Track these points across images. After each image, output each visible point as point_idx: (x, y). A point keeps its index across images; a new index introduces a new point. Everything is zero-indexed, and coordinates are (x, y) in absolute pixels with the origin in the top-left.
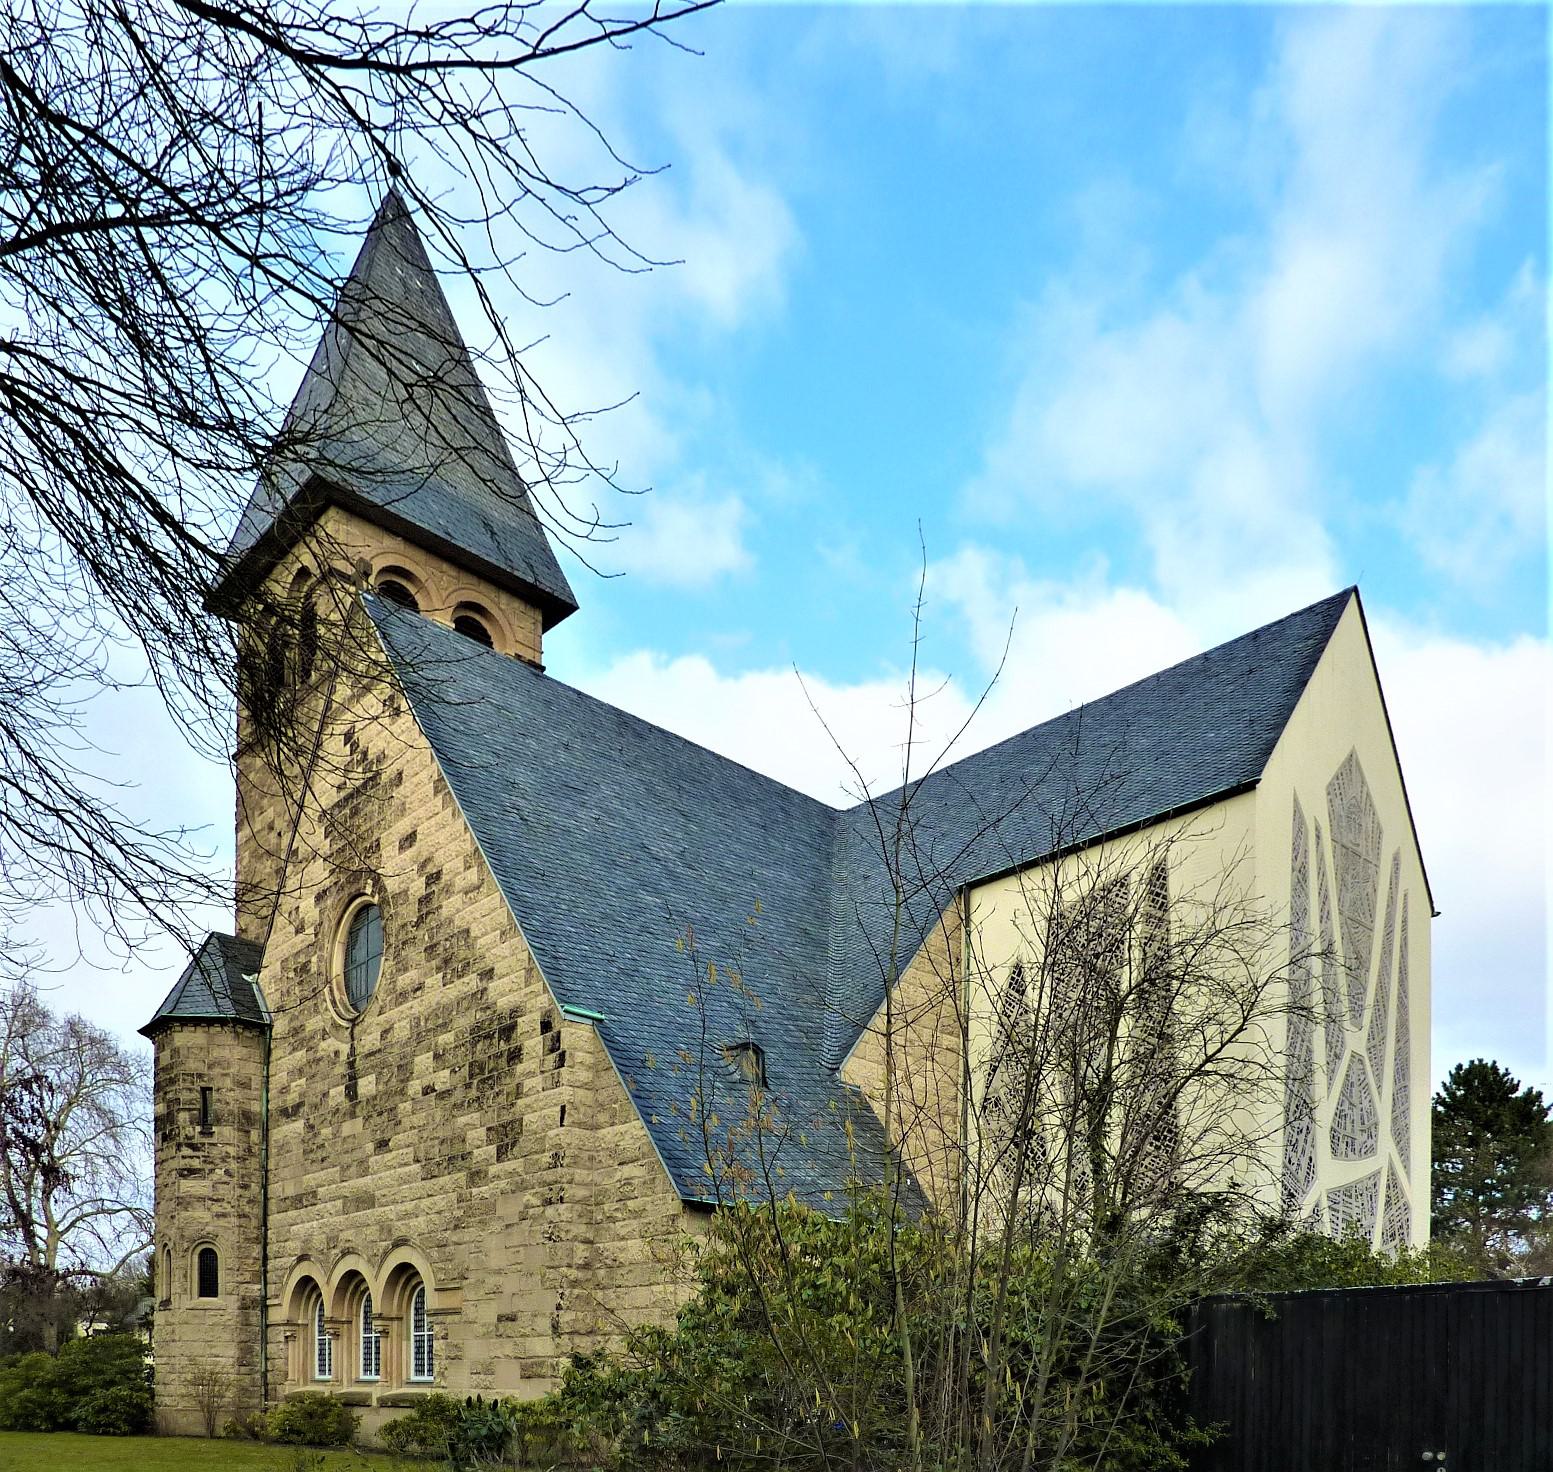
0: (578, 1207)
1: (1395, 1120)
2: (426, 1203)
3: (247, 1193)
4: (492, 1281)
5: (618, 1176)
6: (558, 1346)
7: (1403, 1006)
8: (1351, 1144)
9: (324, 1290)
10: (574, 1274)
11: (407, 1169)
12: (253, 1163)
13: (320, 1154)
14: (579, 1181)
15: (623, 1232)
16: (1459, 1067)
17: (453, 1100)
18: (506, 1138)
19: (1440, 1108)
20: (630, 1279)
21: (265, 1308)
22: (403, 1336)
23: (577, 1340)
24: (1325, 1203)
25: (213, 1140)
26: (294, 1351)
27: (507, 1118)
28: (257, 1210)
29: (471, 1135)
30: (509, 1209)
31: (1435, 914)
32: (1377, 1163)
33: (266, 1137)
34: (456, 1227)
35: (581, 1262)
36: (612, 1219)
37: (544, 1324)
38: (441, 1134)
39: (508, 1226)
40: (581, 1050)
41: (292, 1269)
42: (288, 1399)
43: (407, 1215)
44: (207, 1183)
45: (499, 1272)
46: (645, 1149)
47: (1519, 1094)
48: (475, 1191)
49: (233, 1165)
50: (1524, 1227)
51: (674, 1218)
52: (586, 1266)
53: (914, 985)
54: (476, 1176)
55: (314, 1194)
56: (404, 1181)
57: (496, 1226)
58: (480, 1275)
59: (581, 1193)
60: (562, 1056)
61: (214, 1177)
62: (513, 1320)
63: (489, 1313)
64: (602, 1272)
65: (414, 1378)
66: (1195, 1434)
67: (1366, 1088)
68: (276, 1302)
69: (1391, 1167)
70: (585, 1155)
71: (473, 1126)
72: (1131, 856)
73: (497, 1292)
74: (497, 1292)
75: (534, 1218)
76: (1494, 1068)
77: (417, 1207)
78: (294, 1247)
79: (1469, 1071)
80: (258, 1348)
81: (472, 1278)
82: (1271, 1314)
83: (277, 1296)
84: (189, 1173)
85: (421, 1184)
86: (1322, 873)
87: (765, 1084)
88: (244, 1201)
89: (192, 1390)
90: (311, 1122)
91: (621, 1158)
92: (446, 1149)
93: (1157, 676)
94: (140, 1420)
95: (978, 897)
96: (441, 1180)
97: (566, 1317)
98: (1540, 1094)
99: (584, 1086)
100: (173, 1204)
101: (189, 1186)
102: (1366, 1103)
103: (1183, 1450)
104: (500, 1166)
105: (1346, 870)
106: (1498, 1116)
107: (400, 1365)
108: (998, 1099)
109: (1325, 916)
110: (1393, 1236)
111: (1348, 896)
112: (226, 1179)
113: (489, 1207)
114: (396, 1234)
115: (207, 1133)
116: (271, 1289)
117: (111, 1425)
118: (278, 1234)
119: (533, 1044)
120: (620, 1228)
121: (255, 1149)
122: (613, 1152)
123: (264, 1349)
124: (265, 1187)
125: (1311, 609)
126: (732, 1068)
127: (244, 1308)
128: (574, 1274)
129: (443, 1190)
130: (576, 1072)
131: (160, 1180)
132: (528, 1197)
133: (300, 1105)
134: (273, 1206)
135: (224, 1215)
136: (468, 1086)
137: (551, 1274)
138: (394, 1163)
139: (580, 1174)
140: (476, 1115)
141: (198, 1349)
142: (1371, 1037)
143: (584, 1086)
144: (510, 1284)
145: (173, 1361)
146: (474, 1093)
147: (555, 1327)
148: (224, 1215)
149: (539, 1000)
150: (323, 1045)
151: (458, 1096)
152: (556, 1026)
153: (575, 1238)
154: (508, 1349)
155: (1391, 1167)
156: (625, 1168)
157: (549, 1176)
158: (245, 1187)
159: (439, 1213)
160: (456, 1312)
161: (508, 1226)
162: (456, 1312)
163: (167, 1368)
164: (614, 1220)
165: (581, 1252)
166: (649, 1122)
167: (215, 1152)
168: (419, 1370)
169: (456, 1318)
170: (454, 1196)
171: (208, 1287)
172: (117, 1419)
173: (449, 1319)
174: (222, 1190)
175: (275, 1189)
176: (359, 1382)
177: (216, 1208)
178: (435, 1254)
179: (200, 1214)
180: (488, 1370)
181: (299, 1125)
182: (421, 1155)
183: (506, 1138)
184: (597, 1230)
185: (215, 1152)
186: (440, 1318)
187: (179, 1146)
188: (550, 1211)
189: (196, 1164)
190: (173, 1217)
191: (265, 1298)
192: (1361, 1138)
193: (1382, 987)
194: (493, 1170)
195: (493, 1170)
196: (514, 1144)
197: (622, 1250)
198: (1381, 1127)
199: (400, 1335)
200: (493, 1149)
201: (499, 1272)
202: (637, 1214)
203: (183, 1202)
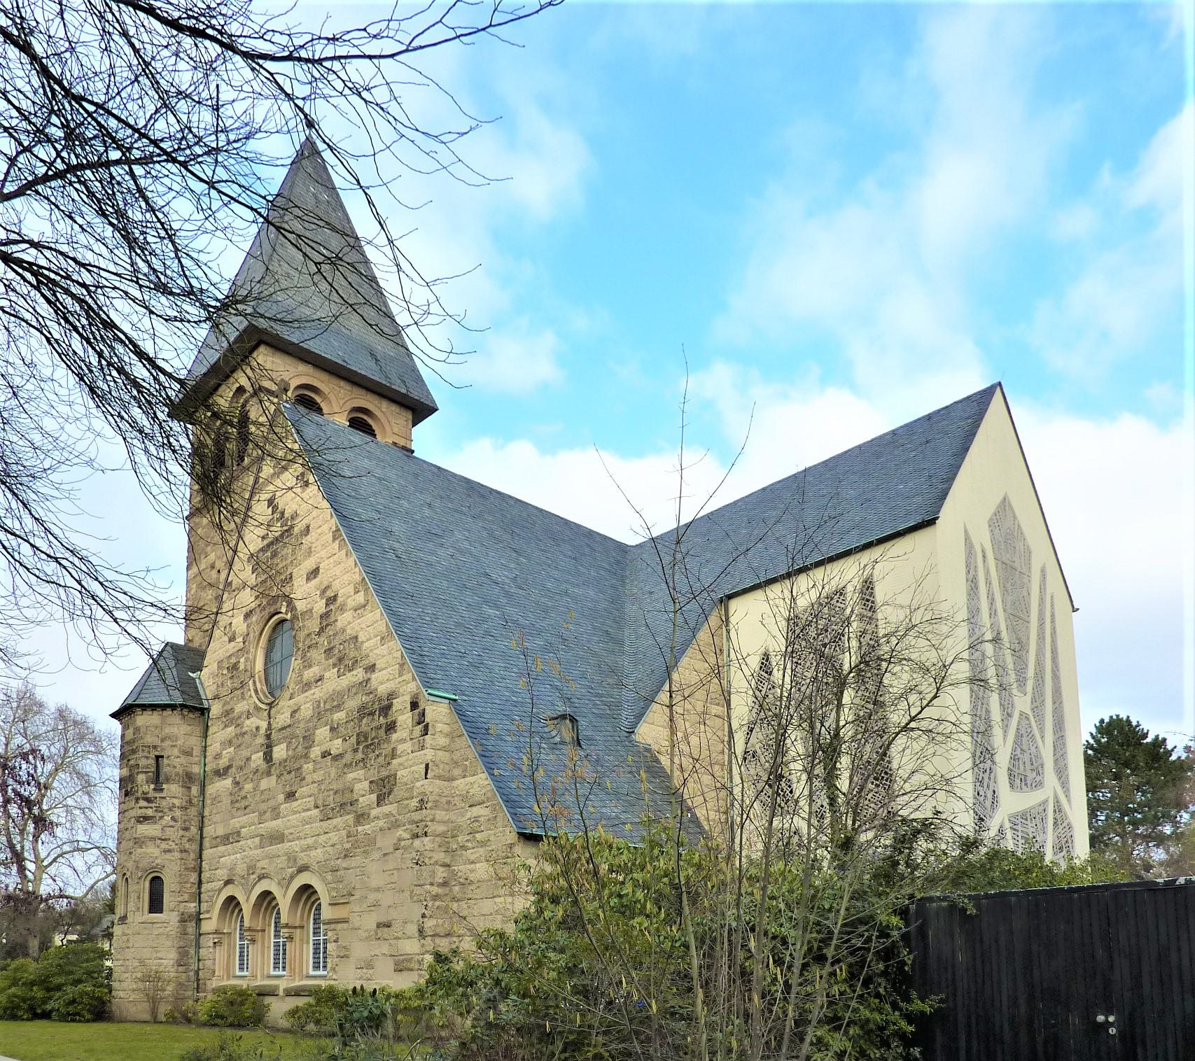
1: (1056, 761)
2: (322, 838)
3: (187, 834)
4: (372, 897)
5: (468, 815)
6: (423, 945)
8: (1024, 780)
12: (193, 811)
14: (439, 820)
15: (472, 858)
16: (1102, 721)
17: (344, 761)
19: (1090, 752)
20: (478, 893)
22: (304, 941)
23: (438, 940)
24: (1007, 825)
26: (220, 954)
27: (384, 773)
28: (195, 847)
29: (357, 787)
30: (386, 842)
31: (1075, 610)
34: (346, 856)
35: (441, 881)
36: (464, 848)
37: (412, 929)
40: (441, 722)
41: (220, 890)
42: (215, 991)
43: (309, 848)
44: (157, 827)
45: (378, 890)
46: (489, 795)
47: (1149, 740)
48: (360, 828)
49: (178, 813)
50: (1161, 840)
51: (511, 846)
52: (445, 884)
54: (361, 818)
55: (238, 833)
56: (306, 822)
57: (376, 855)
59: (441, 828)
61: (163, 822)
63: (370, 921)
64: (457, 888)
65: (312, 973)
66: (918, 1005)
68: (207, 916)
70: (444, 800)
71: (360, 781)
72: (847, 573)
73: (376, 905)
74: (376, 905)
75: (405, 848)
76: (1128, 721)
77: (316, 842)
78: (222, 874)
79: (1110, 724)
80: (192, 952)
81: (358, 895)
84: (144, 819)
86: (988, 583)
87: (579, 745)
89: (141, 985)
92: (338, 798)
94: (100, 1011)
95: (734, 604)
96: (335, 821)
97: (429, 924)
98: (1164, 740)
99: (443, 749)
100: (131, 843)
101: (144, 829)
103: (909, 1018)
104: (379, 809)
108: (755, 752)
111: (1009, 599)
112: (172, 823)
113: (371, 841)
114: (300, 863)
116: (204, 906)
119: (405, 719)
120: (470, 854)
121: (195, 801)
122: (464, 798)
123: (197, 953)
124: (201, 829)
125: (968, 398)
127: (183, 921)
130: (437, 739)
132: (400, 832)
133: (229, 767)
134: (206, 843)
135: (169, 851)
136: (356, 751)
137: (418, 890)
139: (440, 814)
140: (362, 772)
141: (146, 953)
142: (1034, 700)
143: (443, 749)
145: (127, 963)
146: (360, 755)
148: (169, 851)
149: (409, 686)
150: (248, 722)
151: (348, 758)
152: (422, 705)
154: (385, 949)
156: (474, 809)
157: (416, 816)
158: (186, 829)
160: (345, 921)
161: (385, 855)
162: (345, 921)
163: (123, 969)
165: (441, 873)
167: (164, 803)
168: (316, 967)
169: (345, 925)
170: (344, 833)
171: (156, 904)
172: (83, 1009)
174: (169, 832)
176: (309, 977)
177: (164, 846)
178: (329, 877)
179: (152, 850)
180: (370, 966)
181: (227, 782)
182: (320, 803)
183: (384, 788)
184: (452, 856)
185: (164, 803)
187: (137, 800)
188: (417, 842)
189: (150, 812)
191: (199, 913)
192: (1031, 775)
193: (1039, 663)
194: (374, 813)
196: (389, 793)
197: (472, 871)
198: (1046, 767)
199: (301, 940)
200: (374, 797)
201: (378, 890)
202: (483, 844)
203: (139, 842)
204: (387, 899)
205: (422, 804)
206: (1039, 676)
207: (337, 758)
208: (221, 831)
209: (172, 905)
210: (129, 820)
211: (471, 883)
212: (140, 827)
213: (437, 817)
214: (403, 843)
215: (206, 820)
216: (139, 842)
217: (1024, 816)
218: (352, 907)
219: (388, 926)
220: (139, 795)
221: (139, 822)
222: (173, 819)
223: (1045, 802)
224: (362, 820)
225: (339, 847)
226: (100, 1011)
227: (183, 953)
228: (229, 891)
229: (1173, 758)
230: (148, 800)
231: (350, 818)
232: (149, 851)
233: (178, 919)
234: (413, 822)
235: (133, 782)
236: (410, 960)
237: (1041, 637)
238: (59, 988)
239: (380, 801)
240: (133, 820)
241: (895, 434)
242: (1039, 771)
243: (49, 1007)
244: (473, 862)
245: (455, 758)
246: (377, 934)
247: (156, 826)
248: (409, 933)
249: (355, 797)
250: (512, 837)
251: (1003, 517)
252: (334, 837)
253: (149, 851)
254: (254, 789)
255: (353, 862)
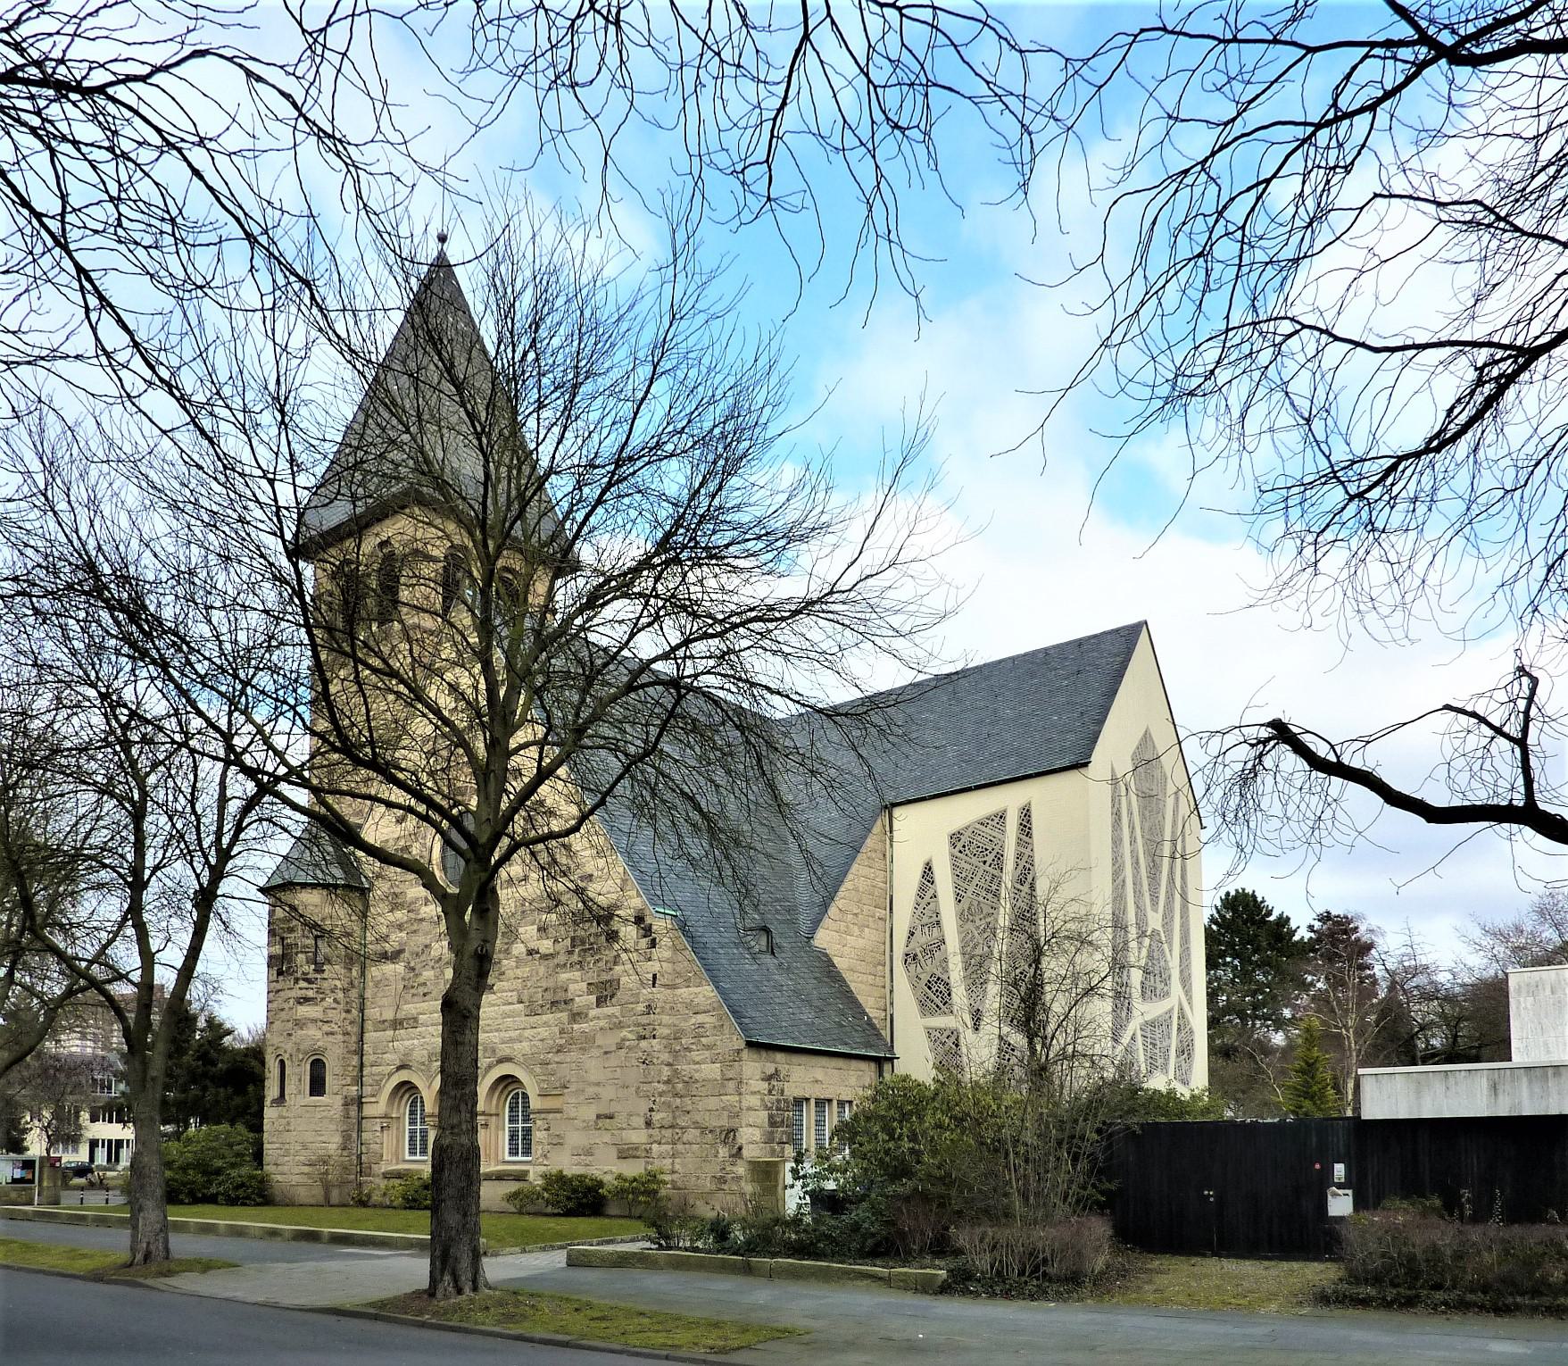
0: (664, 1041)
1: (1181, 971)
2: (528, 1033)
3: (349, 1016)
4: (591, 1091)
5: (693, 1021)
6: (651, 1136)
7: (1183, 877)
8: (1153, 991)
9: (425, 1093)
10: (662, 1087)
11: (511, 1007)
12: (354, 993)
13: (422, 990)
14: (665, 1023)
15: (697, 1059)
16: (1228, 894)
17: (556, 961)
18: (605, 992)
19: (1214, 927)
20: (703, 1091)
21: (360, 1104)
22: (500, 1128)
23: (663, 1131)
24: (1139, 1033)
25: (325, 976)
26: (388, 1139)
27: (605, 977)
28: (355, 1029)
29: (572, 987)
30: (610, 1041)
32: (1170, 1003)
33: (363, 974)
34: (558, 1051)
36: (688, 1049)
37: (641, 1122)
38: (545, 985)
39: (606, 1053)
41: (390, 1075)
42: (388, 1176)
43: (511, 1040)
44: (319, 1008)
45: (598, 1084)
46: (715, 1005)
47: (1272, 918)
48: (576, 1026)
49: (340, 995)
50: (1280, 1024)
51: (739, 1051)
52: (668, 1082)
53: (859, 876)
54: (576, 1016)
55: (415, 1019)
56: (506, 1015)
57: (595, 1052)
58: (581, 1086)
59: (666, 1031)
60: (654, 940)
61: (325, 1004)
62: (611, 1117)
63: (589, 1113)
64: (680, 1086)
65: (508, 1158)
66: (1107, 1186)
67: (1163, 952)
68: (373, 1100)
69: (1180, 1004)
70: (668, 1006)
71: (576, 983)
72: (1009, 799)
73: (597, 1097)
74: (597, 1097)
75: (630, 1048)
76: (1254, 896)
77: (520, 1035)
78: (393, 1058)
79: (1235, 897)
80: (355, 1135)
81: (573, 1088)
82: (1139, 1132)
83: (373, 1096)
84: (305, 1000)
85: (524, 1018)
86: (1130, 813)
87: (773, 953)
88: (347, 1022)
89: (306, 1169)
90: (412, 964)
91: (696, 1009)
92: (549, 996)
93: (1013, 659)
94: (259, 1194)
95: (897, 812)
96: (544, 1018)
97: (657, 1117)
98: (1288, 919)
99: (667, 961)
100: (290, 1025)
101: (304, 1011)
102: (1162, 963)
103: (1102, 1193)
104: (599, 1010)
105: (1145, 808)
106: (1256, 936)
107: (497, 1148)
108: (915, 955)
109: (1133, 841)
110: (1183, 1052)
111: (1147, 825)
112: (335, 1005)
113: (588, 1041)
114: (500, 1054)
115: (319, 970)
116: (367, 1090)
117: (248, 1198)
118: (375, 1048)
119: (629, 932)
120: (695, 1055)
121: (356, 983)
122: (688, 1005)
123: (359, 1136)
124: (362, 1011)
125: (1117, 631)
126: (753, 943)
127: (346, 1104)
128: (662, 1087)
129: (546, 1024)
130: (663, 952)
131: (274, 1005)
132: (624, 1033)
133: (400, 952)
134: (369, 1025)
135: (332, 1034)
136: (570, 953)
137: (645, 1087)
138: (498, 1002)
139: (666, 1019)
140: (578, 974)
141: (309, 1137)
142: (1165, 916)
143: (667, 961)
144: (608, 1093)
145: (287, 1146)
146: (575, 958)
147: (648, 1124)
148: (332, 1034)
149: (635, 901)
150: (424, 909)
151: (562, 959)
152: (648, 920)
153: (662, 1063)
154: (607, 1138)
155: (1180, 1004)
156: (699, 1016)
157: (644, 1019)
158: (348, 1011)
159: (542, 1040)
160: (558, 1111)
161: (606, 1053)
162: (558, 1111)
163: (281, 1152)
164: (690, 1050)
165: (666, 1071)
166: (717, 988)
167: (325, 985)
168: (514, 1152)
169: (558, 1115)
170: (556, 1030)
171: (317, 1087)
172: (253, 1193)
173: (551, 1116)
174: (331, 1014)
175: (372, 1013)
176: (505, 1162)
177: (326, 1028)
178: (538, 1069)
179: (313, 1032)
180: (589, 1153)
181: (400, 967)
182: (525, 998)
183: (605, 992)
184: (675, 1057)
185: (325, 985)
186: (543, 1116)
187: (297, 980)
188: (643, 1044)
189: (310, 994)
190: (290, 1035)
191: (361, 1097)
192: (1160, 986)
193: (1171, 880)
194: (592, 1013)
195: (592, 1013)
196: (612, 997)
197: (697, 1071)
198: (1173, 979)
199: (497, 1127)
200: (593, 998)
201: (598, 1084)
202: (708, 1047)
203: (299, 1024)
204: (608, 1093)
205: (649, 1009)
206: (1170, 897)
207: (545, 957)
208: (389, 1015)
209: (336, 1088)
210: (287, 1000)
211: (697, 1081)
212: (299, 1007)
213: (664, 1022)
214: (627, 1043)
215: (368, 1004)
216: (299, 1024)
217: (1152, 1024)
218: (566, 1098)
219: (611, 1117)
220: (299, 975)
221: (300, 1003)
222: (335, 1000)
223: (1171, 1010)
224: (577, 1018)
225: (551, 1042)
226: (259, 1194)
227: (346, 1137)
228: (403, 1076)
229: (1296, 938)
230: (309, 981)
231: (564, 1016)
232: (311, 1032)
233: (342, 1102)
234: (639, 1025)
235: (290, 961)
236: (636, 1149)
237: (1171, 880)
238: (218, 1172)
239: (600, 1002)
240: (292, 1001)
241: (1047, 654)
242: (1166, 982)
243: (213, 1190)
244: (698, 1063)
245: (678, 969)
246: (596, 1124)
247: (317, 1008)
248: (635, 1125)
249: (570, 996)
250: (743, 1045)
251: (1146, 761)
252: (544, 1032)
253: (311, 1032)
254: (437, 977)
255: (568, 1057)
